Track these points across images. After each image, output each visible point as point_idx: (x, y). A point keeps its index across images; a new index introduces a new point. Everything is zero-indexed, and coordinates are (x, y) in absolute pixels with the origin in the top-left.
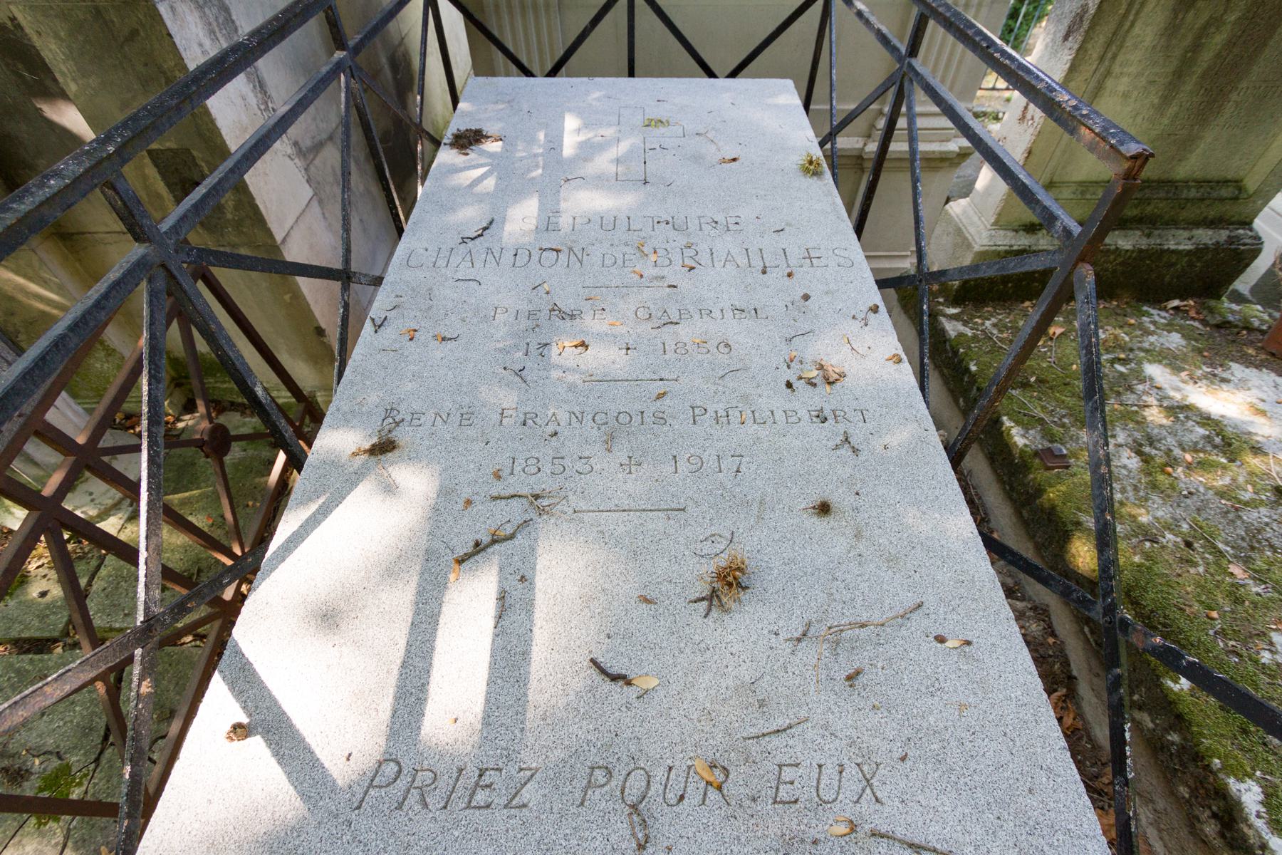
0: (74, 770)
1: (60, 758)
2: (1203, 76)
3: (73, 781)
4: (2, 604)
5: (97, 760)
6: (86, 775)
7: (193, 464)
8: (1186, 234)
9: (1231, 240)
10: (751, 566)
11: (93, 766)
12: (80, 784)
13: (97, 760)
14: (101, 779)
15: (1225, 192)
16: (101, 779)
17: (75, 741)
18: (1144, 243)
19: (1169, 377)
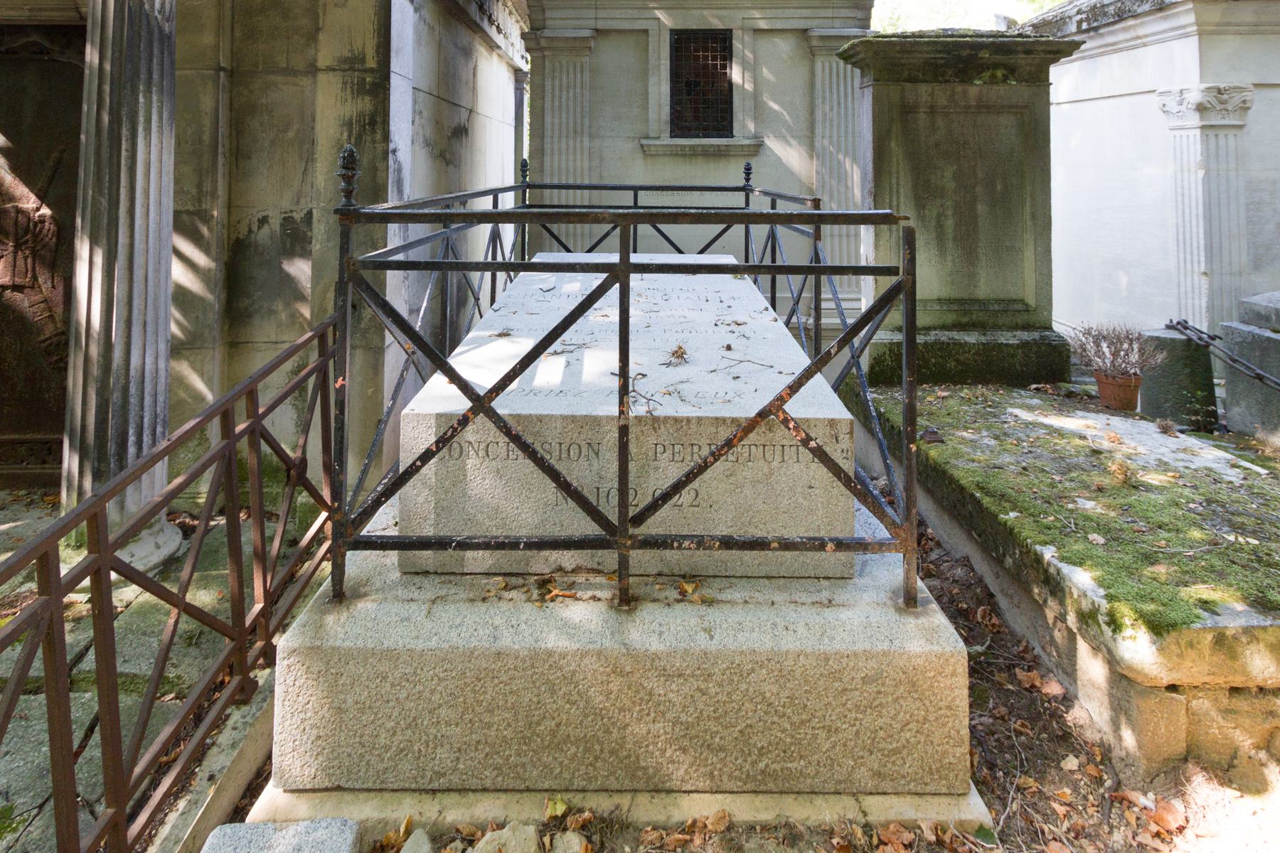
0: (16, 812)
1: (7, 799)
2: (955, 239)
3: (10, 825)
4: (1276, 295)
5: (41, 807)
6: (26, 820)
7: (216, 552)
8: (1009, 334)
9: (1042, 338)
10: (899, 610)
11: (35, 811)
12: (15, 830)
13: (41, 807)
14: (37, 828)
15: (1017, 307)
16: (37, 828)
17: (29, 781)
18: (983, 339)
19: (285, 636)
